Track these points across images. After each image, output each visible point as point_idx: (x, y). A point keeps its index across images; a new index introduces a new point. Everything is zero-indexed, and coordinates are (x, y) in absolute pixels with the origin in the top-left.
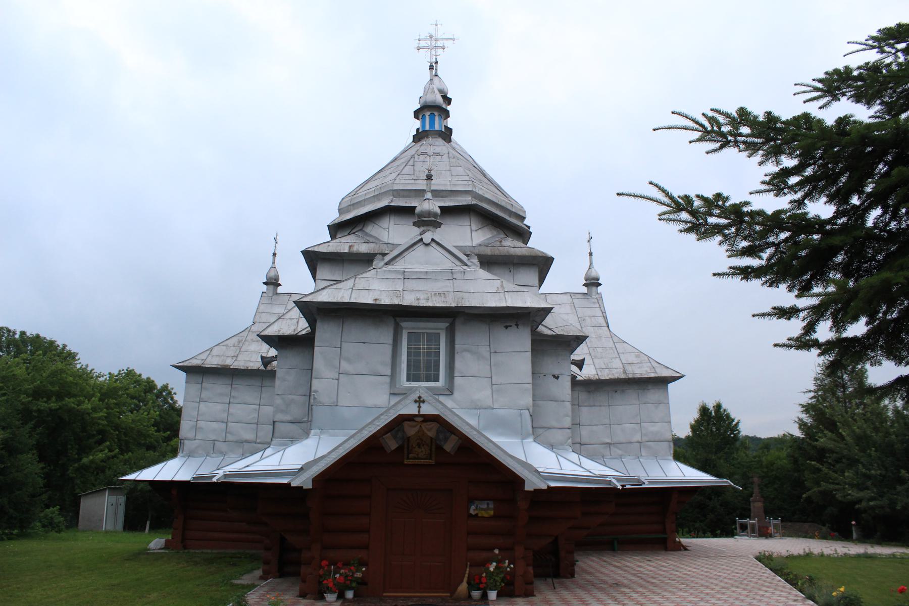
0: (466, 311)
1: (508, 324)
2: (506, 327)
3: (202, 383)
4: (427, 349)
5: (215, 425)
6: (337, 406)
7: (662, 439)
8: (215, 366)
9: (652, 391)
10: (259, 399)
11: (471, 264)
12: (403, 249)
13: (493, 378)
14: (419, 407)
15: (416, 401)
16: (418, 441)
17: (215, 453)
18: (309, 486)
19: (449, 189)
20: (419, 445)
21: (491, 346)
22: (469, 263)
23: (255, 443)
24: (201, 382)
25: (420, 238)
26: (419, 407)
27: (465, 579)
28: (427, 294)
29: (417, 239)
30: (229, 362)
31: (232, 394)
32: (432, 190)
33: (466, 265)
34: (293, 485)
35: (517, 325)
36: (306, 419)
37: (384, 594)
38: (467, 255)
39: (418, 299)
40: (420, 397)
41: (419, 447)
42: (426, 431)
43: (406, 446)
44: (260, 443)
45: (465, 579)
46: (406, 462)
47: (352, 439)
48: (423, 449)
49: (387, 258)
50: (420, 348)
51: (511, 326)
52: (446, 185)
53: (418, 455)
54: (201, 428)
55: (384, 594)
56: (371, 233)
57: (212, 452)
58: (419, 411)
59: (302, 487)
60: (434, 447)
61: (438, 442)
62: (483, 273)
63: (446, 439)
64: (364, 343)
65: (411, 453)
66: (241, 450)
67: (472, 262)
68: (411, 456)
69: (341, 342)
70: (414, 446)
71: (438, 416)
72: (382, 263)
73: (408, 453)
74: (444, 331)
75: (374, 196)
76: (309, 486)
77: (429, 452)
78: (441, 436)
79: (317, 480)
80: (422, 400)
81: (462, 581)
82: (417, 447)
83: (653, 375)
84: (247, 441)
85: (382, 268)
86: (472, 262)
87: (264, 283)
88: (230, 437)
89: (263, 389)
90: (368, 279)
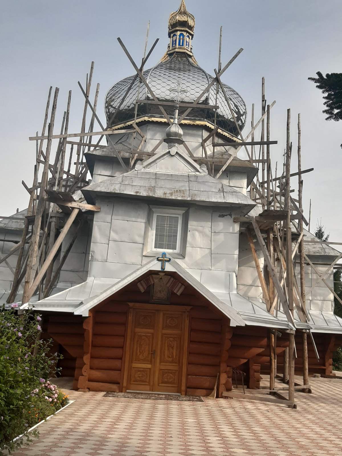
0: (197, 203)
11: (202, 171)
25: (168, 151)
29: (166, 152)
33: (199, 171)
34: (76, 313)
39: (165, 193)
67: (203, 170)
86: (203, 170)
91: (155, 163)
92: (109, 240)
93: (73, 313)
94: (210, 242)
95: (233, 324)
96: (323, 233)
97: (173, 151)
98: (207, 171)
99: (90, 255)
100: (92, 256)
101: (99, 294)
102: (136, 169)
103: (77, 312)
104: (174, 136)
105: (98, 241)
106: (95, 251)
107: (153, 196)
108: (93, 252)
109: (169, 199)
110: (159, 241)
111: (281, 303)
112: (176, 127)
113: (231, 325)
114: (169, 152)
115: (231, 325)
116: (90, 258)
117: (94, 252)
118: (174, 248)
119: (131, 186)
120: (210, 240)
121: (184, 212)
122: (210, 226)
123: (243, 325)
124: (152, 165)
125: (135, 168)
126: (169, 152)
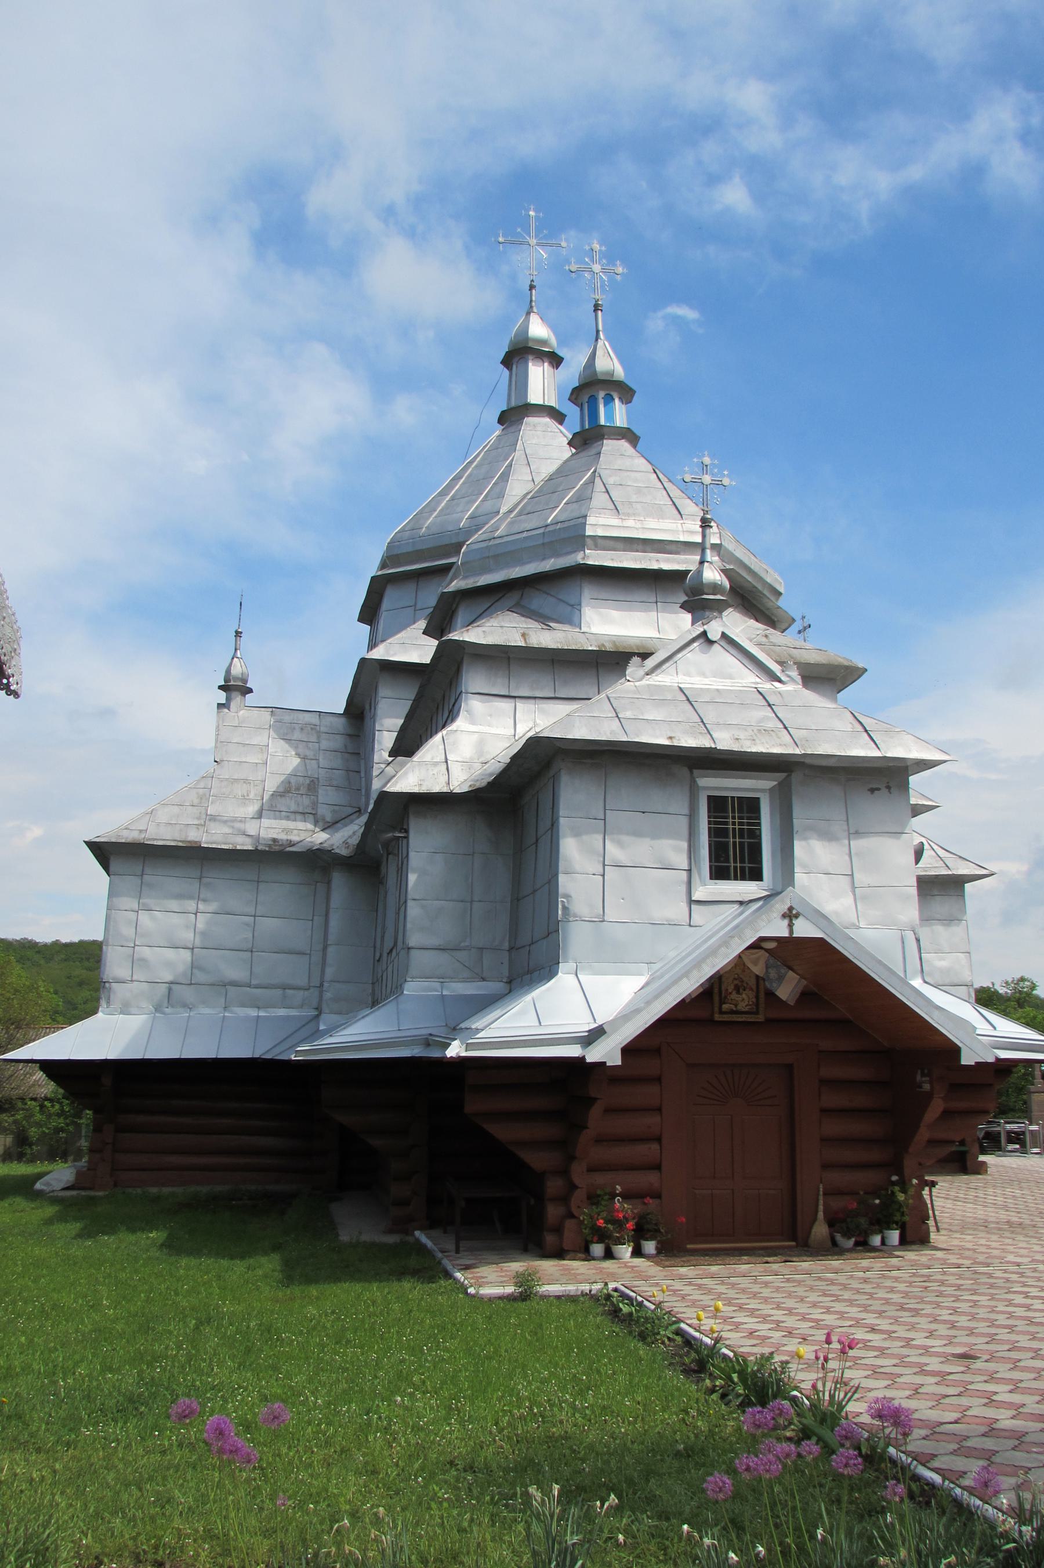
0: (808, 761)
1: (874, 786)
2: (872, 790)
3: (142, 875)
4: (726, 823)
5: (170, 954)
6: (603, 921)
7: (956, 981)
8: (173, 844)
9: (938, 898)
10: (254, 903)
11: (788, 679)
12: (678, 647)
13: (855, 875)
14: (791, 926)
15: (784, 916)
16: (736, 982)
17: (173, 1007)
18: (615, 1060)
19: (682, 539)
20: (737, 989)
21: (850, 821)
22: (783, 678)
23: (249, 987)
24: (140, 873)
25: (702, 630)
26: (791, 926)
27: (821, 1215)
28: (746, 730)
29: (698, 632)
30: (193, 836)
31: (202, 896)
32: (712, 544)
33: (780, 681)
34: (589, 1060)
35: (888, 788)
36: (467, 944)
37: (689, 1246)
38: (781, 663)
39: (737, 739)
40: (791, 909)
41: (738, 992)
42: (750, 965)
43: (716, 990)
44: (257, 987)
45: (821, 1215)
46: (717, 1017)
47: (685, 980)
48: (744, 996)
49: (650, 663)
50: (726, 823)
51: (878, 789)
52: (676, 532)
53: (736, 1006)
54: (143, 960)
55: (689, 1246)
56: (540, 611)
57: (166, 1004)
58: (791, 932)
59: (605, 1063)
60: (762, 995)
61: (768, 984)
62: (810, 697)
63: (781, 978)
64: (644, 812)
65: (725, 1003)
66: (223, 1000)
67: (789, 676)
68: (725, 1007)
69: (605, 810)
70: (730, 991)
71: (821, 940)
72: (641, 672)
73: (721, 1003)
74: (767, 795)
75: (543, 544)
76: (615, 1060)
77: (754, 1000)
78: (773, 974)
79: (627, 1051)
80: (794, 912)
81: (815, 1219)
82: (734, 993)
83: (944, 872)
84: (234, 984)
85: (641, 680)
86: (789, 676)
87: (220, 687)
88: (200, 977)
89: (262, 886)
90: (632, 700)
91: (671, 662)
92: (604, 865)
93: (584, 1058)
94: (847, 858)
95: (967, 1059)
96: (383, 877)
97: (714, 630)
98: (799, 679)
99: (560, 906)
100: (565, 908)
101: (642, 1005)
102: (628, 678)
103: (593, 1055)
104: (711, 592)
105: (577, 867)
106: (573, 894)
107: (713, 746)
108: (567, 896)
109: (751, 752)
110: (728, 861)
111: (477, 1036)
112: (713, 571)
113: (963, 1062)
114: (704, 634)
115: (963, 1062)
116: (560, 912)
117: (570, 897)
118: (756, 875)
119: (513, 734)
120: (847, 851)
121: (775, 783)
122: (845, 819)
123: (991, 1059)
124: (664, 667)
125: (625, 676)
126: (704, 634)
